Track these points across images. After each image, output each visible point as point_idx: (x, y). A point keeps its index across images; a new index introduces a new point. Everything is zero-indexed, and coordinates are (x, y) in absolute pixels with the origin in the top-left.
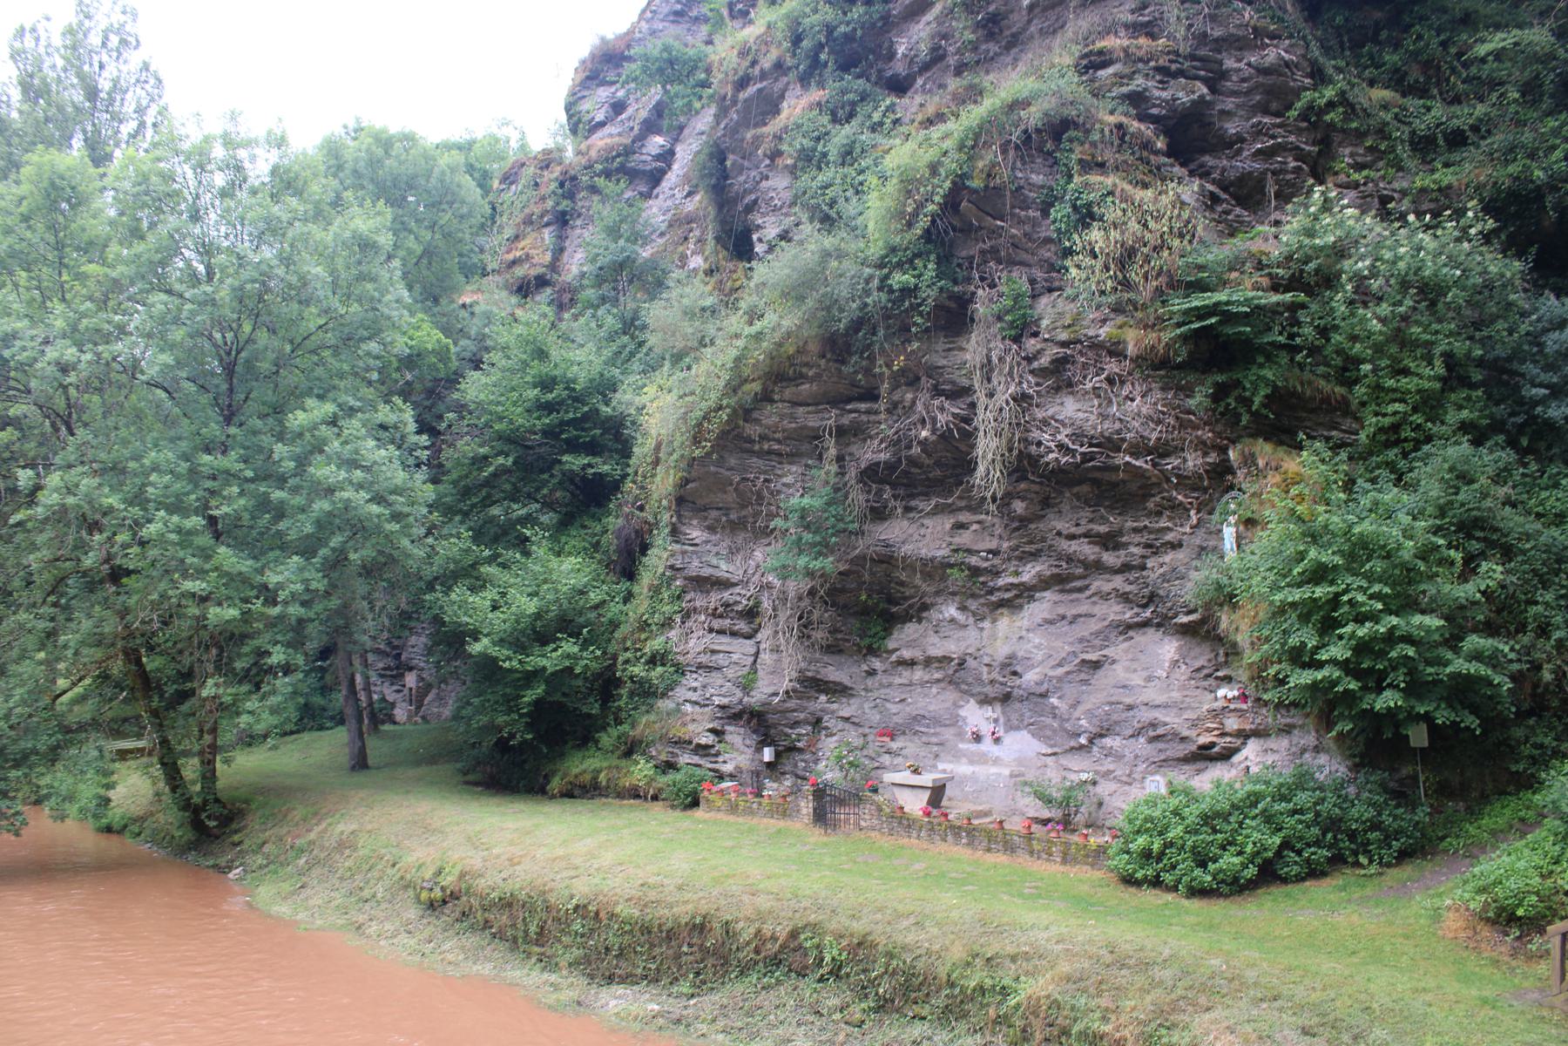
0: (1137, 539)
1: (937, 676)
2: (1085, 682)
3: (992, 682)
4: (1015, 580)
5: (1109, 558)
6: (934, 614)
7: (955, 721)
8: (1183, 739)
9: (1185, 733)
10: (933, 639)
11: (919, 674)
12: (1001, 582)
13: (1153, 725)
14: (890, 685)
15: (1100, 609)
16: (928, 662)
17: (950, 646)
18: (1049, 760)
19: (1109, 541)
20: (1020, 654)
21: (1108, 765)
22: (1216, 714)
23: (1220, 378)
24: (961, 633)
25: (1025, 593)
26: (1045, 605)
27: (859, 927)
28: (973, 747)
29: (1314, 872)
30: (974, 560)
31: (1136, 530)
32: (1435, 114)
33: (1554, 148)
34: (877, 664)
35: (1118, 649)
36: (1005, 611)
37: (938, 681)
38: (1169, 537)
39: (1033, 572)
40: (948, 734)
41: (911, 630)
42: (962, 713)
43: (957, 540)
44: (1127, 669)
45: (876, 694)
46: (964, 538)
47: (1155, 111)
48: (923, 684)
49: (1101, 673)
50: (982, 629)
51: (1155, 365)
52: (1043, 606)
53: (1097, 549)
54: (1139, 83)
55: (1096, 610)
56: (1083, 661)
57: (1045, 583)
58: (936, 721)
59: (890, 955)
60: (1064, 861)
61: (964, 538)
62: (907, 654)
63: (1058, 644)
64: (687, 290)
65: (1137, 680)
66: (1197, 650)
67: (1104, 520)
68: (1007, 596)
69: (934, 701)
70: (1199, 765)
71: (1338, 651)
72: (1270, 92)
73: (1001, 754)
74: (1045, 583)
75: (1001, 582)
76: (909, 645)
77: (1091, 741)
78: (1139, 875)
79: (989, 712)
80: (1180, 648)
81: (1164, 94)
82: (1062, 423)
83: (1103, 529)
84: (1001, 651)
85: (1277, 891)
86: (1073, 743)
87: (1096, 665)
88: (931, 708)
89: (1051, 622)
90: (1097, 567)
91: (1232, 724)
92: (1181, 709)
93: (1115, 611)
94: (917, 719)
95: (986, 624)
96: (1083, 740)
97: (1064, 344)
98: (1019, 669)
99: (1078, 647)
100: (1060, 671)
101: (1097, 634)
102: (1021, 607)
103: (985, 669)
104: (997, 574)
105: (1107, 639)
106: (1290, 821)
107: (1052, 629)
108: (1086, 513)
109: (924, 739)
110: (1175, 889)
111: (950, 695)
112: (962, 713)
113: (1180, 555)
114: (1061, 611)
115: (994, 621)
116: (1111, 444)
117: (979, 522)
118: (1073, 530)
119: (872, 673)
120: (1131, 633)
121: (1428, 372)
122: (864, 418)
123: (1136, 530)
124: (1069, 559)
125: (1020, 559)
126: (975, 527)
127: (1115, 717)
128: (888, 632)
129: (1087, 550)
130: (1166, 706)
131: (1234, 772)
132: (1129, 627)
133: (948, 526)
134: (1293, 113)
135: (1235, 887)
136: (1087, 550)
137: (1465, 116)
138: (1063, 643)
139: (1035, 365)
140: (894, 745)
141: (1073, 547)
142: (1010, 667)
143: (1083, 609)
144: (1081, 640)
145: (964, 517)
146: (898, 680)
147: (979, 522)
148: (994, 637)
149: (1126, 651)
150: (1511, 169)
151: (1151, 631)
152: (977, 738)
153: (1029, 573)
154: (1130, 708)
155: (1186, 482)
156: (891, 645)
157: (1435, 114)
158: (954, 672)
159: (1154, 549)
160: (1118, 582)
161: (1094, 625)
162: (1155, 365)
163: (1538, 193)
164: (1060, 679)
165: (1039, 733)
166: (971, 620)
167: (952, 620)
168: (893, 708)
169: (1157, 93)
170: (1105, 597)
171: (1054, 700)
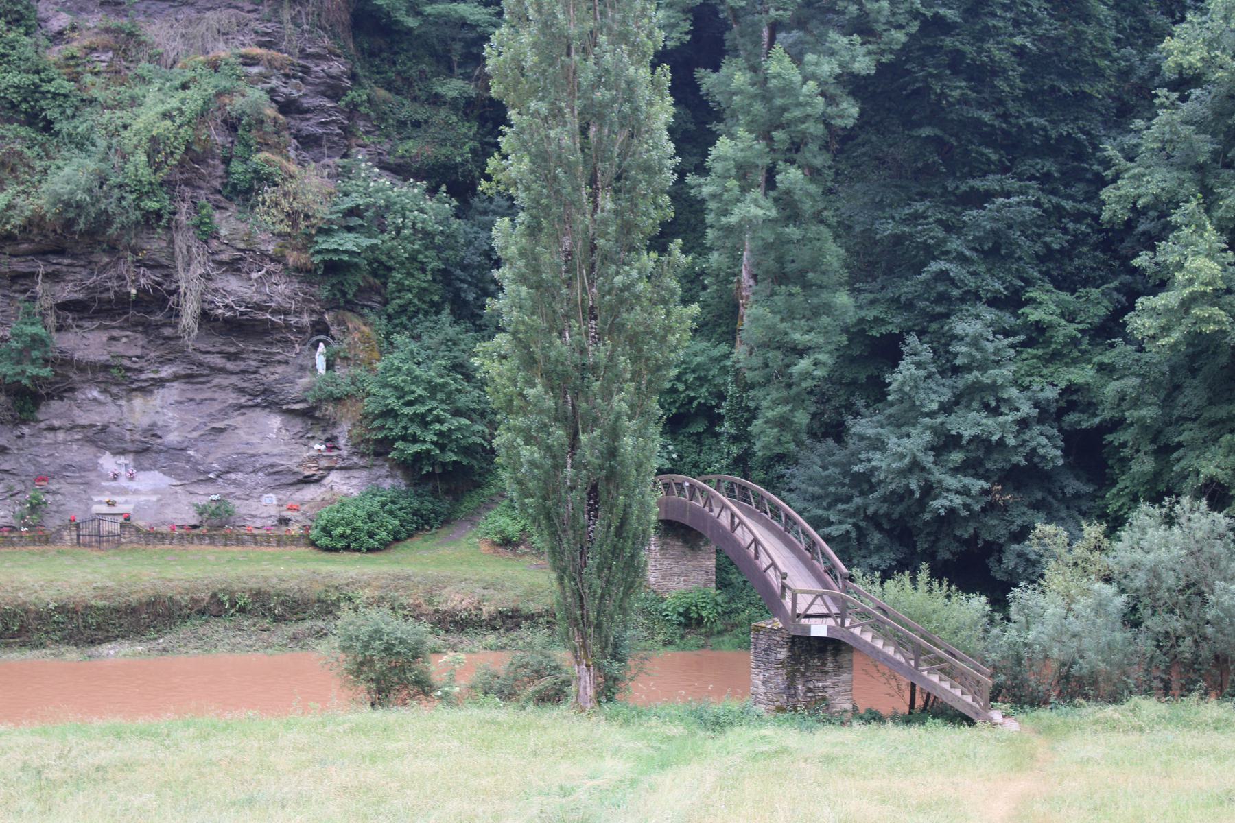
0: (254, 356)
1: (77, 437)
2: (213, 441)
3: (133, 441)
4: (152, 375)
5: (230, 366)
6: (79, 396)
7: (95, 467)
8: (294, 473)
9: (296, 470)
10: (77, 412)
11: (61, 436)
12: (143, 377)
13: (272, 466)
14: (38, 444)
15: (220, 395)
16: (74, 427)
17: (96, 417)
18: (177, 489)
19: (231, 357)
20: (160, 423)
21: (231, 489)
22: (312, 458)
23: (334, 281)
24: (102, 409)
25: (160, 383)
26: (174, 391)
27: (255, 586)
28: (114, 484)
29: (410, 535)
30: (127, 363)
31: (255, 351)
32: (408, 110)
33: (464, 144)
34: (26, 430)
35: (236, 420)
36: (138, 393)
37: (78, 440)
38: (279, 357)
39: (170, 371)
40: (92, 476)
41: (56, 404)
42: (100, 461)
43: (113, 349)
44: (248, 433)
45: (27, 452)
46: (119, 348)
47: (278, 99)
48: (65, 442)
49: (225, 435)
50: (120, 406)
51: (304, 273)
52: (173, 392)
53: (224, 361)
54: (274, 82)
55: (216, 396)
56: (214, 428)
57: (176, 378)
58: (82, 468)
59: (278, 595)
60: (278, 545)
61: (119, 348)
62: (56, 423)
63: (189, 416)
64: (396, 363)
65: (255, 439)
66: (294, 422)
67: (233, 344)
68: (144, 384)
69: (78, 454)
70: (299, 486)
71: (431, 437)
72: (330, 86)
73: (139, 487)
74: (176, 378)
75: (143, 377)
76: (56, 417)
77: (218, 476)
78: (339, 546)
79: (122, 460)
80: (282, 421)
81: (285, 90)
82: (229, 293)
83: (232, 350)
84: (145, 422)
85: (401, 544)
86: (201, 477)
87: (222, 430)
88: (77, 459)
89: (181, 403)
90: (222, 371)
91: (324, 463)
92: (290, 456)
93: (232, 398)
94: (65, 468)
95: (123, 402)
96: (212, 476)
97: (243, 251)
98: (159, 433)
99: (206, 419)
100: (195, 434)
101: (220, 411)
102: (151, 392)
103: (128, 433)
104: (140, 371)
105: (226, 414)
106: (400, 513)
107: (181, 407)
108: (220, 339)
109: (69, 480)
110: (359, 550)
111: (89, 451)
112: (100, 461)
113: (289, 370)
114: (190, 395)
115: (129, 400)
116: (259, 307)
117: (127, 337)
118: (211, 349)
119: (21, 437)
120: (243, 411)
121: (422, 276)
122: (65, 269)
123: (255, 351)
124: (200, 365)
125: (161, 363)
126: (124, 340)
127: (241, 461)
128: (37, 406)
129: (219, 361)
130: (281, 455)
131: (323, 489)
132: (242, 407)
133: (105, 339)
134: (342, 103)
135: (384, 546)
136: (219, 361)
137: (422, 113)
138: (196, 417)
139: (217, 257)
140: (53, 487)
141: (209, 359)
142: (152, 431)
143: (208, 395)
144: (209, 415)
145: (116, 333)
146: (44, 441)
147: (127, 337)
148: (132, 411)
149: (244, 422)
150: (443, 151)
151: (258, 410)
152: (116, 477)
153: (166, 372)
154: (253, 456)
155: (301, 330)
156: (40, 416)
157: (408, 110)
158: (100, 438)
159: (265, 363)
160: (234, 379)
161: (217, 406)
162: (304, 273)
163: (456, 166)
164: (196, 440)
165: (170, 472)
166: (109, 399)
167: (95, 400)
168: (45, 461)
169: (282, 89)
170: (222, 388)
171: (191, 453)
